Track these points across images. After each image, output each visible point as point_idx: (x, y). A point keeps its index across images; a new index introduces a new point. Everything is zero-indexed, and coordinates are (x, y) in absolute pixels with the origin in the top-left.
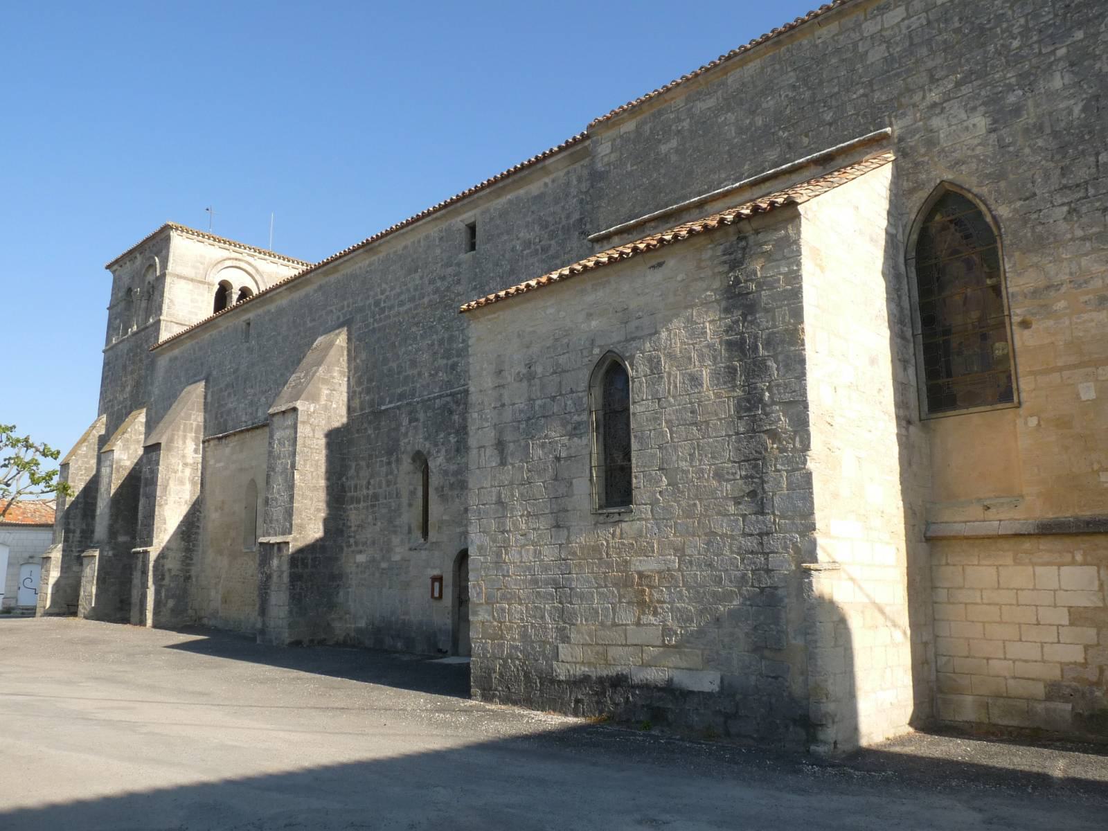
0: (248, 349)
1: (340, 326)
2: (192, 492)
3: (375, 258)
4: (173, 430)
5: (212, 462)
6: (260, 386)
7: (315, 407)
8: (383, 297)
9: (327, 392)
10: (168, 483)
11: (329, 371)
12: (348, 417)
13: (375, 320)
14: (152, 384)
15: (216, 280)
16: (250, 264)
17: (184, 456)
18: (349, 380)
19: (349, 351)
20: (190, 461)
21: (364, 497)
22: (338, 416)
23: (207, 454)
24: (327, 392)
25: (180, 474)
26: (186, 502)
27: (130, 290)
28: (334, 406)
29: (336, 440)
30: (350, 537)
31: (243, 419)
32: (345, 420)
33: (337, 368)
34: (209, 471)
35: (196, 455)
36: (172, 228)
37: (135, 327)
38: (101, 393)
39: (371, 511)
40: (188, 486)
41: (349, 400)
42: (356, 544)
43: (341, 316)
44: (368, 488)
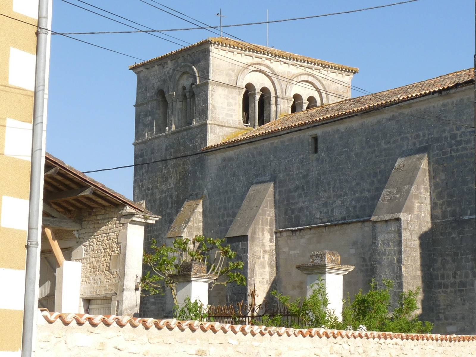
0: (317, 159)
1: (422, 150)
2: (271, 274)
3: (449, 101)
4: (255, 225)
5: (285, 249)
6: (334, 191)
7: (411, 217)
8: (459, 133)
9: (417, 205)
10: (254, 267)
11: (418, 189)
12: (432, 223)
13: (452, 150)
14: (203, 178)
15: (243, 84)
16: (268, 67)
17: (263, 245)
18: (430, 195)
19: (429, 173)
20: (267, 248)
21: (451, 284)
22: (427, 225)
23: (280, 243)
24: (417, 205)
25: (261, 259)
26: (267, 282)
27: (161, 93)
28: (423, 215)
29: (427, 241)
30: (440, 313)
31: (318, 217)
32: (430, 226)
33: (423, 186)
34: (282, 257)
35: (271, 244)
36: (211, 43)
37: (174, 126)
38: (135, 181)
39: (458, 294)
40: (267, 269)
41: (431, 211)
42: (446, 318)
43: (417, 144)
44: (455, 278)
